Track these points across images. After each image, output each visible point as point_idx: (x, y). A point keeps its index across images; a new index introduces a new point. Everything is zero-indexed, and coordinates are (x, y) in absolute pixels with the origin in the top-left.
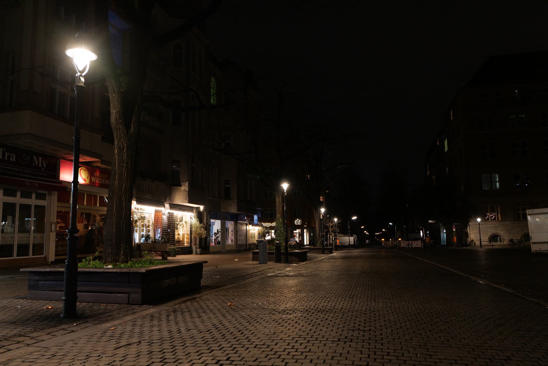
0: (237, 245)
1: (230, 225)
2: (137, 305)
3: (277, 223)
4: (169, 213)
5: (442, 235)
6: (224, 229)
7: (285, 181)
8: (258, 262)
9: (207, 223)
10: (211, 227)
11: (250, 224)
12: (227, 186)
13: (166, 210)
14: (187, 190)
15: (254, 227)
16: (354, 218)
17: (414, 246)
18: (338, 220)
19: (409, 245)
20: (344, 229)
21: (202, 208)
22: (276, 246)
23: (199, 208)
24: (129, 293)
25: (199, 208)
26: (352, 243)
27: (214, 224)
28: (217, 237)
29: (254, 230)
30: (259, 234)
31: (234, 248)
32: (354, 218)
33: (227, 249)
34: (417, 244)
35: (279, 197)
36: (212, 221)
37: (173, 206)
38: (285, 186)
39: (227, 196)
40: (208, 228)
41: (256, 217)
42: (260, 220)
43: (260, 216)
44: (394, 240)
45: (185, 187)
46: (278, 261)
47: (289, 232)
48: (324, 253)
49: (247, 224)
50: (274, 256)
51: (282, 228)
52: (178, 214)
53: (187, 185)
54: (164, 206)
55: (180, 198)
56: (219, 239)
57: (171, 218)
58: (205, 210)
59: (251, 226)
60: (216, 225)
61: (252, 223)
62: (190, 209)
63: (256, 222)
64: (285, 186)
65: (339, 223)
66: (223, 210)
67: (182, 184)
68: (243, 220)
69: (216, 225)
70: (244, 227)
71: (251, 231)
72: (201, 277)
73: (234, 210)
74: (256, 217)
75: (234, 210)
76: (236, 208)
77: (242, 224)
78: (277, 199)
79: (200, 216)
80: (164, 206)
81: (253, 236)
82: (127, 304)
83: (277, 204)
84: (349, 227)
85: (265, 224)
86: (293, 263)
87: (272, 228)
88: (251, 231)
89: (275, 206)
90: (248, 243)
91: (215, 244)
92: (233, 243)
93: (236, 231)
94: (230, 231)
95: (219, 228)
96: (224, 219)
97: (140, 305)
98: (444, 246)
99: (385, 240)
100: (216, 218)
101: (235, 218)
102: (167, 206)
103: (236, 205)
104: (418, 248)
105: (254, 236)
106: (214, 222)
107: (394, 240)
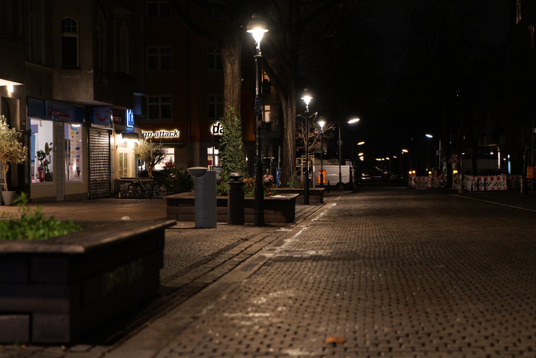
0: (90, 183)
2: (59, 345)
6: (60, 142)
7: (257, 21)
8: (193, 225)
9: (23, 127)
10: (32, 138)
11: (118, 132)
12: (66, 35)
15: (126, 140)
16: (354, 121)
17: (489, 188)
18: (327, 125)
19: (478, 185)
22: (231, 184)
24: (30, 314)
26: (346, 180)
28: (46, 163)
29: (126, 148)
30: (137, 156)
31: (84, 190)
32: (354, 121)
33: (68, 192)
35: (232, 63)
36: (34, 122)
38: (258, 33)
39: (70, 62)
40: (26, 136)
41: (129, 115)
42: (142, 123)
43: (139, 113)
44: (438, 174)
46: (237, 219)
47: (197, 152)
49: (110, 133)
50: (228, 209)
51: (240, 141)
56: (50, 167)
59: (120, 136)
60: (43, 133)
63: (130, 126)
64: (258, 33)
65: (327, 132)
68: (103, 121)
69: (43, 133)
70: (104, 140)
71: (120, 150)
72: (162, 266)
73: (85, 95)
74: (129, 115)
75: (85, 95)
76: (91, 91)
77: (99, 133)
78: (229, 68)
82: (27, 344)
84: (340, 142)
85: (149, 134)
86: (279, 227)
87: (169, 143)
88: (120, 150)
91: (42, 180)
92: (80, 179)
93: (87, 150)
94: (73, 148)
95: (50, 139)
96: (60, 115)
97: (68, 346)
99: (417, 174)
100: (43, 117)
101: (88, 116)
103: (91, 84)
104: (499, 192)
105: (126, 160)
106: (36, 126)
107: (438, 174)
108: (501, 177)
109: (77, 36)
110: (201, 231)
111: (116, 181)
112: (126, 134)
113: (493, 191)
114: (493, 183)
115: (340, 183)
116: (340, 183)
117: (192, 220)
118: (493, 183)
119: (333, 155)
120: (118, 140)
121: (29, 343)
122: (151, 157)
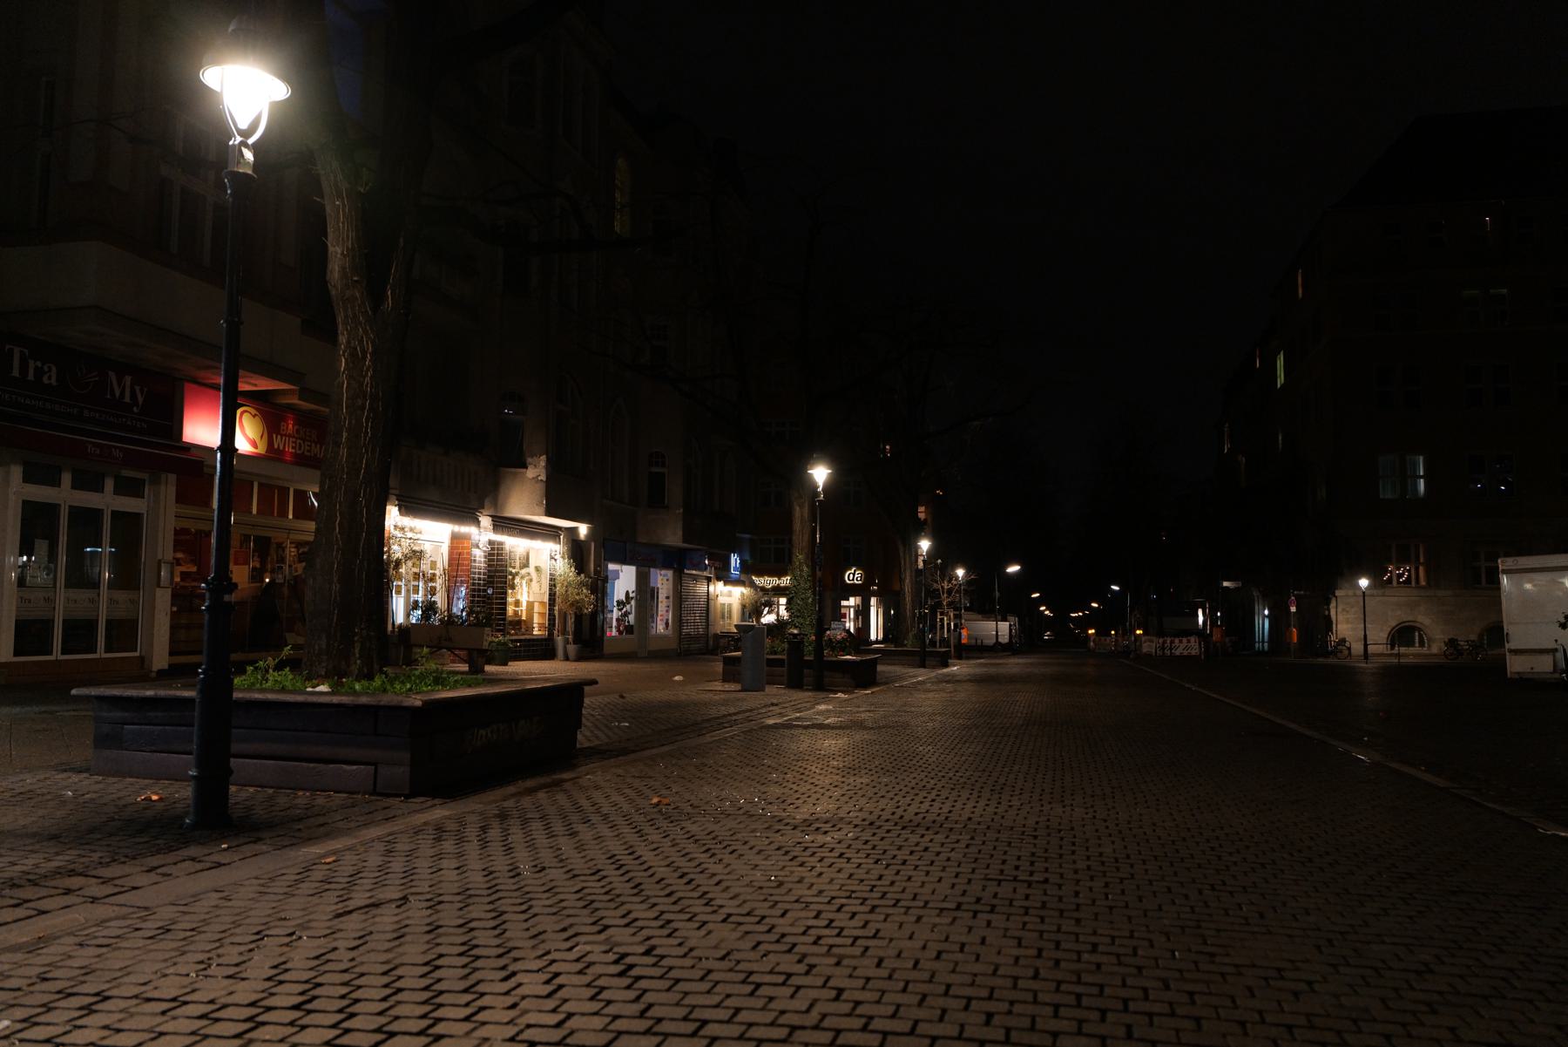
1: (662, 580)
3: (794, 578)
4: (491, 543)
5: (1258, 621)
6: (645, 593)
8: (738, 687)
11: (719, 579)
12: (655, 470)
13: (481, 534)
14: (543, 477)
15: (729, 588)
16: (1013, 569)
17: (1178, 653)
20: (982, 598)
21: (583, 530)
23: (574, 531)
24: (375, 764)
25: (574, 531)
26: (1004, 639)
27: (617, 575)
28: (626, 614)
29: (729, 596)
30: (744, 607)
31: (674, 645)
32: (1013, 569)
34: (1188, 647)
35: (801, 507)
36: (611, 567)
37: (503, 524)
38: (820, 474)
39: (657, 499)
40: (600, 585)
41: (735, 560)
44: (1124, 634)
45: (536, 471)
46: (795, 683)
48: (924, 666)
49: (709, 580)
52: (515, 545)
53: (543, 464)
54: (477, 523)
55: (523, 502)
56: (631, 618)
57: (496, 556)
58: (592, 534)
59: (721, 584)
60: (624, 580)
61: (723, 575)
62: (551, 533)
64: (820, 474)
65: (968, 582)
66: (642, 539)
67: (529, 460)
69: (624, 580)
71: (721, 600)
72: (579, 725)
73: (673, 537)
75: (673, 537)
76: (680, 533)
77: (695, 578)
79: (577, 552)
80: (477, 523)
81: (726, 613)
83: (797, 526)
85: (760, 581)
87: (778, 591)
88: (721, 600)
89: (789, 530)
90: (712, 631)
91: (620, 632)
92: (669, 632)
93: (680, 598)
94: (662, 596)
95: (632, 587)
96: (644, 562)
97: (407, 797)
98: (1262, 653)
101: (678, 562)
102: (486, 521)
103: (680, 525)
104: (1189, 657)
105: (730, 612)
107: (1124, 634)
108: (1192, 639)
109: (665, 470)
110: (743, 694)
111: (716, 635)
112: (728, 581)
113: (1181, 657)
114: (1182, 646)
115: (997, 642)
116: (997, 642)
117: (735, 681)
118: (1182, 646)
119: (986, 610)
120: (718, 588)
121: (374, 793)
122: (753, 610)
